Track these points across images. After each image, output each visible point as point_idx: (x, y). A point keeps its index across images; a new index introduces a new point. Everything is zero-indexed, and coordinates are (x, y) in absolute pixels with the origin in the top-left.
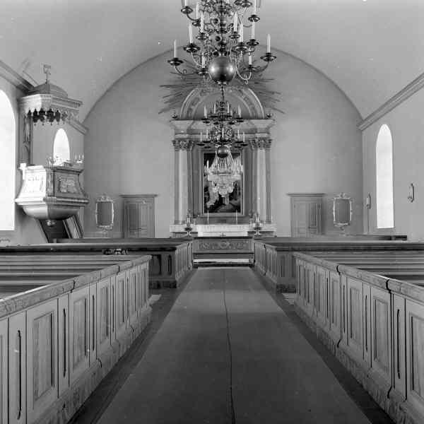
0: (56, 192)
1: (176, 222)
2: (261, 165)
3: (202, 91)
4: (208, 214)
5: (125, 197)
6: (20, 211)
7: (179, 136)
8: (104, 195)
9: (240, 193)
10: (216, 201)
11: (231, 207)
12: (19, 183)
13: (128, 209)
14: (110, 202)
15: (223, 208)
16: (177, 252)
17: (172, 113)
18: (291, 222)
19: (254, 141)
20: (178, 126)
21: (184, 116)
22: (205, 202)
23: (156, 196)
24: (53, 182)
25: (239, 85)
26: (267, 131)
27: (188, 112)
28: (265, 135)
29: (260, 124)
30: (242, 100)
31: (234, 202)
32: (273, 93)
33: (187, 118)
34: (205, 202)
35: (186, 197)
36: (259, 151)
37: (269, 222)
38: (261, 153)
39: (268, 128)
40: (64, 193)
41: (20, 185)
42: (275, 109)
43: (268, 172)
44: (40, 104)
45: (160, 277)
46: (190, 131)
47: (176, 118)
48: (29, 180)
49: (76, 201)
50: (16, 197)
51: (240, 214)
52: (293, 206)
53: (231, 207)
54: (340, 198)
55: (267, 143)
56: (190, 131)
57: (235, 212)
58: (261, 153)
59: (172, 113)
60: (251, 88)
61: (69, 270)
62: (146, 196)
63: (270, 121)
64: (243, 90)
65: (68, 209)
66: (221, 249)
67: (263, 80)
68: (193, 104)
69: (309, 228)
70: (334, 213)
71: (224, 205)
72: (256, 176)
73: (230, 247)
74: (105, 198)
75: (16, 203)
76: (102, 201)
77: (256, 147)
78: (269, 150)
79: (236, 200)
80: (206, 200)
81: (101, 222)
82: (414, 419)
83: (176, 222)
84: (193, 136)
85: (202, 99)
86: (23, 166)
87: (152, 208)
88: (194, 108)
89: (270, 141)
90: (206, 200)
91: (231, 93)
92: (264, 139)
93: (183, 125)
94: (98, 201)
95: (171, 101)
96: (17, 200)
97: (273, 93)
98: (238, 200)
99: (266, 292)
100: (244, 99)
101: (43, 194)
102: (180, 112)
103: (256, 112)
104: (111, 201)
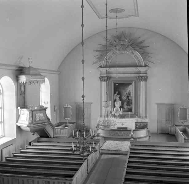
0: (33, 121)
1: (101, 116)
3: (113, 53)
5: (77, 103)
6: (19, 128)
7: (102, 75)
8: (67, 104)
9: (132, 103)
12: (18, 117)
14: (70, 107)
16: (73, 181)
17: (98, 65)
19: (139, 78)
20: (102, 71)
21: (105, 65)
24: (32, 117)
27: (107, 63)
28: (145, 75)
29: (142, 69)
30: (133, 57)
31: (129, 107)
32: (149, 53)
33: (106, 67)
37: (146, 117)
38: (142, 83)
39: (146, 71)
40: (37, 121)
41: (18, 117)
42: (150, 62)
43: (146, 93)
44: (25, 79)
46: (108, 73)
47: (101, 67)
48: (22, 114)
49: (44, 124)
50: (17, 122)
51: (131, 113)
52: (159, 110)
54: (182, 108)
55: (145, 79)
56: (108, 73)
57: (129, 112)
63: (147, 68)
66: (119, 135)
67: (144, 47)
69: (167, 120)
70: (179, 115)
73: (124, 135)
74: (67, 105)
75: (17, 125)
76: (66, 107)
77: (140, 80)
78: (147, 82)
79: (130, 106)
81: (66, 117)
83: (101, 116)
84: (109, 75)
85: (113, 56)
86: (19, 108)
87: (90, 108)
89: (147, 77)
91: (128, 54)
92: (144, 76)
93: (104, 70)
94: (64, 107)
95: (98, 58)
96: (17, 124)
97: (149, 53)
100: (134, 56)
101: (27, 123)
102: (103, 63)
103: (140, 63)
104: (70, 107)
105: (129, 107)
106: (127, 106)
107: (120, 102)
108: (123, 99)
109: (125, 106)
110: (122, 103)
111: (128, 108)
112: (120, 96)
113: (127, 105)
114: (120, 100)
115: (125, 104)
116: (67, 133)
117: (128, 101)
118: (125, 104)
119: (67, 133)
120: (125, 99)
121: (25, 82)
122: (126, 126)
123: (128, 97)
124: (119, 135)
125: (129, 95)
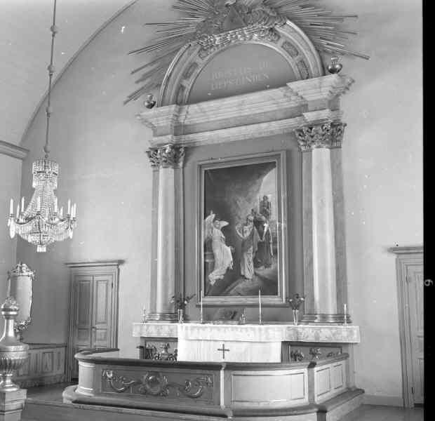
2: (321, 208)
5: (74, 266)
9: (275, 252)
10: (228, 269)
13: (78, 288)
15: (240, 286)
18: (402, 314)
23: (121, 262)
25: (267, 18)
26: (333, 105)
27: (177, 93)
28: (325, 114)
31: (263, 271)
36: (315, 151)
37: (341, 318)
55: (333, 134)
58: (320, 155)
59: (143, 100)
60: (291, 20)
61: (225, 162)
62: (105, 263)
64: (277, 28)
68: (186, 76)
71: (244, 277)
72: (310, 212)
79: (268, 266)
87: (116, 285)
88: (188, 84)
90: (208, 268)
97: (341, 18)
98: (273, 267)
99: (314, 119)
105: (263, 271)
106: (256, 264)
107: (229, 249)
109: (248, 270)
110: (233, 254)
112: (225, 223)
113: (255, 260)
115: (249, 258)
117: (260, 244)
118: (249, 258)
120: (248, 234)
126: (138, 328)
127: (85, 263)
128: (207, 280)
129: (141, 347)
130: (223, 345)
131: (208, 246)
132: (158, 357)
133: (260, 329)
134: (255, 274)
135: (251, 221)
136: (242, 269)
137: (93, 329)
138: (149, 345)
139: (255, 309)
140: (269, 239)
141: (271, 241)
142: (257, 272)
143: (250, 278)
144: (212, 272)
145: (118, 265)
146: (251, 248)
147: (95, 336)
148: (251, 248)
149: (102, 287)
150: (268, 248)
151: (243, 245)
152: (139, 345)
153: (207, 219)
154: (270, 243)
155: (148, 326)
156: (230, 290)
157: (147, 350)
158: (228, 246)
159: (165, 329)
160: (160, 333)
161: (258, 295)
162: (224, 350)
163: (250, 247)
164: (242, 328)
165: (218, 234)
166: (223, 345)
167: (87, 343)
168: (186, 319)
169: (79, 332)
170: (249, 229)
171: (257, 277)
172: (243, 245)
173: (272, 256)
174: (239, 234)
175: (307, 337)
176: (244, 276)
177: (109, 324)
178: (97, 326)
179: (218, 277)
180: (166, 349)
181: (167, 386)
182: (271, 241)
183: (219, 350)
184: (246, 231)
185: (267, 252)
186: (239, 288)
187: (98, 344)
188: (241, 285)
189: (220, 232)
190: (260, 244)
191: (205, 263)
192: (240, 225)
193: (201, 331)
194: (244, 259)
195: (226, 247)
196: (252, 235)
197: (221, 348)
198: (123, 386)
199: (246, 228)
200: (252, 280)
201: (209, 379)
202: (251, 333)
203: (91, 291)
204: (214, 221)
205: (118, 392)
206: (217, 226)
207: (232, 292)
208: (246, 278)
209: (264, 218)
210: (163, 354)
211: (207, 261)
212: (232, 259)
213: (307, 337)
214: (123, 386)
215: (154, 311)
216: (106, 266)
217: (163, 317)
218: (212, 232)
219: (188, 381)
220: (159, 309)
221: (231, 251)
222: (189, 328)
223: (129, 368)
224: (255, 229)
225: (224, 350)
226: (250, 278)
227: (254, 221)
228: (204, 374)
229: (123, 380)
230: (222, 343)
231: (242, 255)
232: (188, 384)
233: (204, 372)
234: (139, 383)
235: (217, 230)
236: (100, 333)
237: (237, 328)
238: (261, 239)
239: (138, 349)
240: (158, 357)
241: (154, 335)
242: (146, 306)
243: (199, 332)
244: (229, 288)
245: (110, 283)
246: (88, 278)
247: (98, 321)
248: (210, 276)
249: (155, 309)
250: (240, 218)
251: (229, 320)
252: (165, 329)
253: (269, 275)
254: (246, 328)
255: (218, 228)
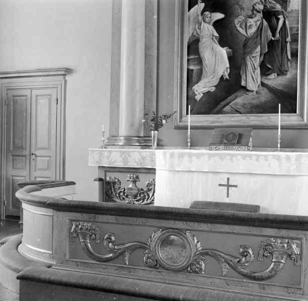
4: (191, 120)
9: (294, 54)
10: (222, 78)
11: (265, 96)
22: (190, 83)
31: (274, 80)
34: (190, 83)
35: (121, 85)
45: (27, 157)
53: (265, 96)
62: (46, 73)
65: (105, 193)
66: (157, 265)
71: (245, 88)
79: (281, 73)
80: (192, 79)
82: (198, 275)
83: (112, 140)
87: (61, 101)
90: (192, 79)
98: (289, 75)
105: (274, 80)
106: (265, 71)
107: (224, 52)
108: (242, 31)
109: (252, 79)
110: (231, 59)
111: (271, 89)
112: (219, 16)
113: (263, 66)
114: (222, 43)
115: (254, 61)
116: (222, 211)
117: (271, 44)
118: (254, 61)
119: (222, 211)
120: (253, 30)
121: (112, 161)
122: (258, 205)
123: (269, 15)
124: (157, 265)
125: (278, 7)
126: (96, 156)
127: (19, 72)
128: (190, 93)
129: (100, 180)
130: (228, 179)
131: (194, 47)
132: (124, 193)
133: (288, 158)
134: (263, 84)
135: (259, 12)
136: (243, 77)
137: (33, 157)
138: (110, 177)
139: (275, 131)
140: (286, 36)
141: (289, 39)
142: (266, 82)
143: (255, 89)
144: (197, 82)
145: (64, 75)
146: (259, 49)
147: (36, 166)
148: (259, 49)
149: (43, 102)
150: (284, 48)
151: (245, 45)
152: (97, 176)
153: (192, 10)
154: (286, 42)
155: (110, 152)
156: (225, 106)
157: (108, 183)
158: (222, 46)
159: (136, 157)
160: (127, 163)
161: (278, 113)
162: (228, 186)
163: (256, 48)
164: (258, 156)
165: (208, 31)
166: (228, 179)
167: (25, 173)
168: (160, 145)
169: (13, 160)
170: (256, 22)
171: (266, 90)
172: (245, 45)
173: (288, 60)
174: (239, 29)
175: (115, 162)
176: (245, 88)
177: (53, 148)
178: (37, 153)
179: (206, 90)
180: (134, 182)
181: (202, 254)
182: (289, 39)
183: (220, 185)
184: (250, 26)
185: (282, 53)
186: (236, 104)
187: (40, 175)
188: (240, 100)
189: (211, 28)
190: (271, 44)
191: (188, 70)
192: (241, 18)
193: (194, 158)
194: (246, 65)
195: (221, 48)
196: (260, 29)
197: (225, 182)
198: (111, 251)
199: (251, 21)
200: (257, 93)
201: (294, 246)
202: (275, 163)
203: (29, 111)
204: (202, 13)
205: (100, 260)
206: (207, 20)
207: (227, 108)
208: (248, 91)
209: (278, 7)
210: (131, 189)
211: (191, 67)
212: (228, 65)
213: (115, 162)
214: (111, 251)
215: (115, 134)
216: (48, 76)
217: (129, 141)
218: (200, 29)
219: (245, 247)
220: (123, 131)
221: (228, 53)
222: (293, 160)
223: (121, 219)
224: (265, 23)
225: (228, 186)
226: (255, 89)
227: (264, 12)
228: (283, 238)
229: (111, 241)
230: (227, 176)
231: (244, 59)
232: (245, 254)
233: (284, 232)
234: (143, 246)
235: (206, 25)
236: (41, 162)
237: (250, 156)
238: (274, 35)
239: (97, 183)
240: (124, 193)
241: (120, 164)
242: (105, 127)
243: (191, 162)
244: (223, 103)
245: (54, 98)
246: (28, 93)
247: (39, 146)
248: (195, 87)
249: (117, 130)
250: (242, 9)
251: (233, 144)
252: (136, 157)
253: (286, 86)
254: (266, 156)
255: (209, 23)
